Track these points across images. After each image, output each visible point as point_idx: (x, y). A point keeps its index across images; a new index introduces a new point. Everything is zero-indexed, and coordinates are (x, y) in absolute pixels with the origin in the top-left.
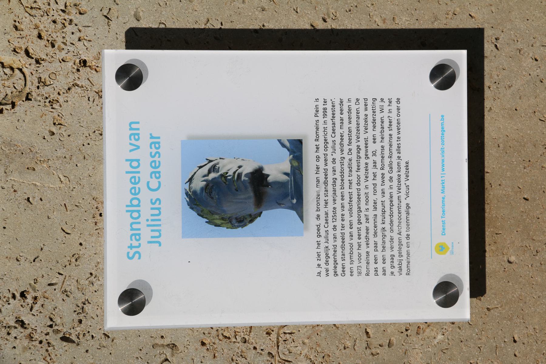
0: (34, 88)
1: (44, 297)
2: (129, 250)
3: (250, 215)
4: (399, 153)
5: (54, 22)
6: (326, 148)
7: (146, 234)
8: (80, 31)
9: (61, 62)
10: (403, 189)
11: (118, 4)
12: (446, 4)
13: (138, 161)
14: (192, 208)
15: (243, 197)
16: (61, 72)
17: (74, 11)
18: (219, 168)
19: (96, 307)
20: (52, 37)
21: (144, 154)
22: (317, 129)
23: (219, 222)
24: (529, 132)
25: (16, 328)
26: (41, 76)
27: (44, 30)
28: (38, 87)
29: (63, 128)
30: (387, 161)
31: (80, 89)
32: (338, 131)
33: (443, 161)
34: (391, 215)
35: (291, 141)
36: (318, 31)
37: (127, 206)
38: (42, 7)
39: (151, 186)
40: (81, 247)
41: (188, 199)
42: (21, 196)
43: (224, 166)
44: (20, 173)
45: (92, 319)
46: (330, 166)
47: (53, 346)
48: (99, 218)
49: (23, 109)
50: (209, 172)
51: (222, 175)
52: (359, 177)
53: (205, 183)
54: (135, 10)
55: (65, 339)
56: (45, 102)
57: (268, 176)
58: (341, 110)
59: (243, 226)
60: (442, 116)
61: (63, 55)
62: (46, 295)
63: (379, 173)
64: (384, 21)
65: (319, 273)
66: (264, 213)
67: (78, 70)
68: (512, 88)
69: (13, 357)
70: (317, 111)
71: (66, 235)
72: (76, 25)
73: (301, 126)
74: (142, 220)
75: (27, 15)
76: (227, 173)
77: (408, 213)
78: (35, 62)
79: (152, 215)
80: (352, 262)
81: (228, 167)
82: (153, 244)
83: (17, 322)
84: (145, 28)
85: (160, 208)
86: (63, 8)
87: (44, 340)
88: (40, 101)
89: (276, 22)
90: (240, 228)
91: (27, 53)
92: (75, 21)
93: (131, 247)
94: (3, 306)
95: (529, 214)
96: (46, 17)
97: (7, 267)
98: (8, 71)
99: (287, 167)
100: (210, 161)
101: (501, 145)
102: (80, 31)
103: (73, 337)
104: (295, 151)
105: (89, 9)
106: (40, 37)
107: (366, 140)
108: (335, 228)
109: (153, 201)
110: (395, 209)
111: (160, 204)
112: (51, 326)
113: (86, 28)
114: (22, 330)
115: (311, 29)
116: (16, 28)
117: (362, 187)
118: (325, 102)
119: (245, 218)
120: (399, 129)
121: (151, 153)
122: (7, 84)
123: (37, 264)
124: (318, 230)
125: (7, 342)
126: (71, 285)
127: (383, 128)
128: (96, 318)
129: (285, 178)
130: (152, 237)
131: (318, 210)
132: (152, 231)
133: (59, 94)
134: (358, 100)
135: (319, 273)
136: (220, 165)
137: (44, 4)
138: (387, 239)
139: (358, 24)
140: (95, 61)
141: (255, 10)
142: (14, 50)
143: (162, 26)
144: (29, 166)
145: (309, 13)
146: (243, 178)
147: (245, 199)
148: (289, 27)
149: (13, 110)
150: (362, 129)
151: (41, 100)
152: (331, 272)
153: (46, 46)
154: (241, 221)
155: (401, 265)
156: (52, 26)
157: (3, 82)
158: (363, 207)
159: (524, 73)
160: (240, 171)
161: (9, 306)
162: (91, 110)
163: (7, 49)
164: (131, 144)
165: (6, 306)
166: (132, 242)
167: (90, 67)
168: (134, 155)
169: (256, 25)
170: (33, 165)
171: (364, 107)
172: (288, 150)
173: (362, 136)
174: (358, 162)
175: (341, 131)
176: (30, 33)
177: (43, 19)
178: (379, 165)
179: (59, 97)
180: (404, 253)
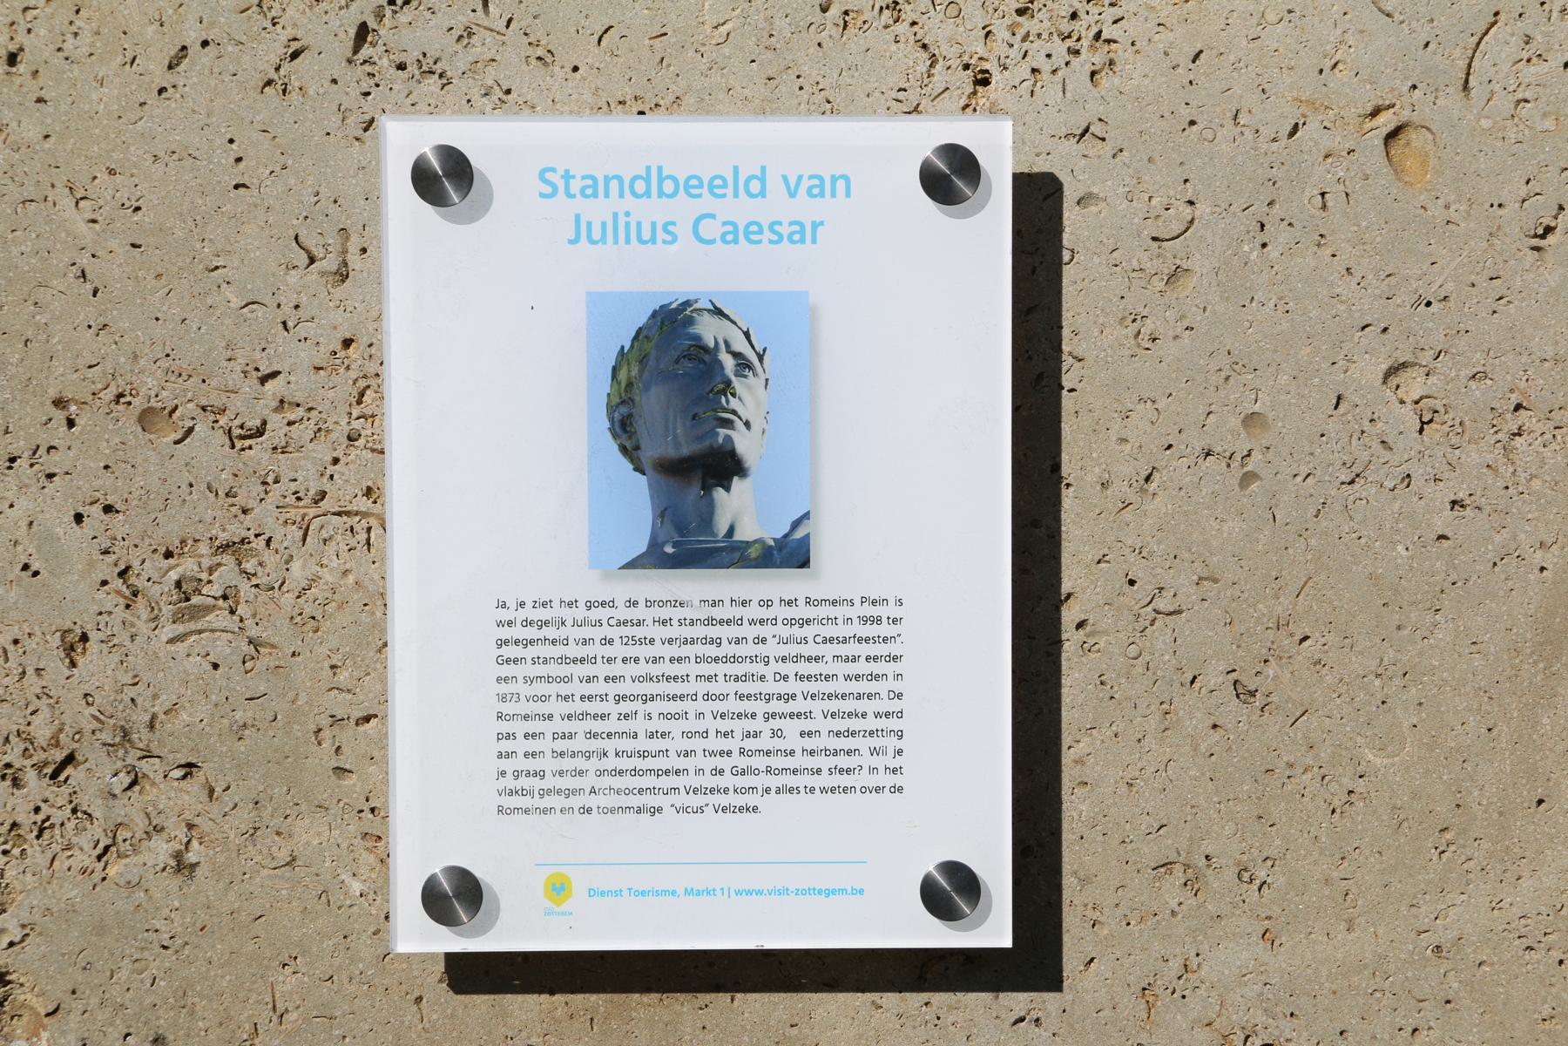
2: (561, 172)
3: (637, 448)
4: (778, 791)
5: (1074, 16)
6: (790, 622)
7: (597, 211)
10: (698, 800)
13: (763, 193)
14: (654, 314)
16: (962, 29)
17: (1099, 59)
19: (433, 102)
21: (777, 207)
22: (834, 603)
23: (623, 375)
29: (836, 32)
30: (760, 762)
32: (829, 650)
33: (759, 892)
34: (635, 772)
35: (805, 542)
36: (1058, 609)
37: (660, 169)
40: (568, 69)
41: (674, 306)
43: (749, 388)
51: (728, 383)
52: (723, 697)
53: (712, 344)
57: (728, 489)
58: (875, 659)
59: (612, 430)
60: (861, 891)
61: (1001, 33)
63: (733, 744)
65: (504, 605)
66: (642, 480)
67: (966, 67)
70: (874, 603)
71: (596, 37)
73: (838, 566)
74: (629, 202)
76: (734, 395)
79: (639, 224)
80: (529, 680)
81: (748, 398)
84: (1061, 218)
86: (1104, 36)
90: (608, 425)
92: (1075, 61)
93: (567, 176)
99: (745, 533)
100: (761, 358)
101: (795, 1031)
103: (366, 51)
107: (808, 715)
109: (671, 228)
110: (648, 781)
117: (701, 706)
119: (631, 435)
120: (833, 790)
121: (780, 223)
124: (603, 604)
126: (483, 46)
129: (722, 529)
130: (589, 224)
131: (649, 603)
132: (604, 225)
133: (914, 23)
134: (899, 696)
135: (504, 605)
136: (751, 379)
143: (1066, 258)
146: (722, 432)
148: (1064, 544)
150: (834, 705)
152: (506, 633)
154: (624, 426)
155: (521, 794)
160: (739, 424)
162: (877, 94)
164: (800, 178)
167: (975, 93)
172: (786, 536)
173: (817, 707)
174: (756, 697)
175: (829, 658)
178: (750, 744)
179: (906, 24)
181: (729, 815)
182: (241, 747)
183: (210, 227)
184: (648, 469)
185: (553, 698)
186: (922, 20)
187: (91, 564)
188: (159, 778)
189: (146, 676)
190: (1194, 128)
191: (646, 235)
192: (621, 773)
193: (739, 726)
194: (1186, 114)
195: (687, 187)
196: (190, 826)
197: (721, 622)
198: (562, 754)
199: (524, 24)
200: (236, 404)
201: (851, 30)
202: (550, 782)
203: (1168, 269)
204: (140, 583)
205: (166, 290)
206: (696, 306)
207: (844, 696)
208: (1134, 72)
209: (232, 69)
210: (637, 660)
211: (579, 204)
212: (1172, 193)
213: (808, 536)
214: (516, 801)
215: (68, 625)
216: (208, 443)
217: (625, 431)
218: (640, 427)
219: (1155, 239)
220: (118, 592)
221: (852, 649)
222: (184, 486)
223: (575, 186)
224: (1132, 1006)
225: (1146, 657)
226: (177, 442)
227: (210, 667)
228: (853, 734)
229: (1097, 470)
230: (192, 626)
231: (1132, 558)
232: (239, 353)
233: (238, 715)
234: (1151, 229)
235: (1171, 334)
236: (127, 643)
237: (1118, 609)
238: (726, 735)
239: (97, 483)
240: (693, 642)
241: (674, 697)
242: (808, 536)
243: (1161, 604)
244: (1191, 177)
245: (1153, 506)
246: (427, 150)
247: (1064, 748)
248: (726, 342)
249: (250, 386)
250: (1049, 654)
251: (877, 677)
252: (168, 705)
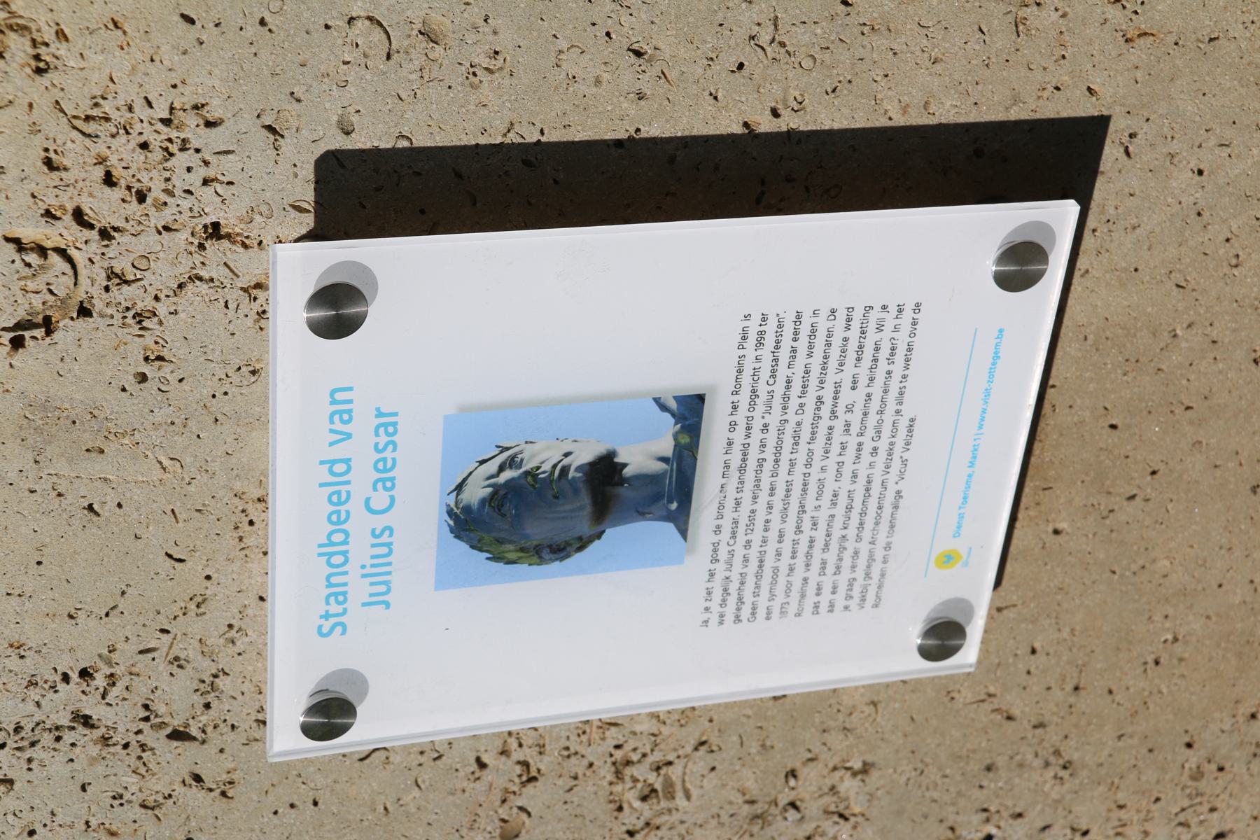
0: (96, 291)
1: (131, 674)
3: (580, 538)
4: (900, 403)
5: (144, 146)
7: (359, 589)
9: (160, 233)
10: (896, 465)
13: (347, 461)
14: (457, 537)
15: (567, 507)
16: (161, 255)
17: (192, 120)
18: (522, 460)
19: (240, 680)
20: (139, 181)
21: (361, 449)
22: (740, 372)
24: (1149, 310)
25: (73, 728)
26: (113, 263)
27: (119, 166)
28: (107, 289)
29: (167, 368)
30: (872, 420)
31: (205, 286)
32: (782, 371)
33: (984, 411)
34: (863, 513)
37: (320, 546)
38: (114, 115)
39: (373, 505)
40: (208, 583)
41: (452, 523)
42: (74, 502)
43: (533, 456)
44: (70, 461)
46: (756, 435)
47: (152, 749)
48: (248, 528)
49: (71, 335)
50: (501, 468)
51: (527, 473)
52: (811, 453)
53: (490, 490)
54: (340, 112)
55: (177, 735)
56: (125, 317)
57: (625, 465)
58: (796, 333)
59: (562, 559)
60: (1001, 331)
61: (167, 216)
62: (134, 670)
63: (852, 442)
64: (905, 110)
65: (706, 622)
67: (202, 247)
68: (1138, 231)
70: (744, 338)
71: (177, 565)
74: (353, 567)
76: (538, 468)
77: (896, 507)
78: (98, 237)
79: (373, 557)
80: (772, 597)
81: (542, 455)
84: (363, 151)
85: (391, 543)
86: (166, 115)
87: (134, 743)
88: (112, 317)
89: (667, 121)
91: (78, 215)
92: (195, 143)
93: (327, 616)
94: (44, 696)
96: (123, 138)
98: (33, 258)
99: (666, 446)
101: (1091, 337)
102: (206, 163)
103: (194, 731)
104: (687, 415)
105: (229, 115)
106: (109, 180)
107: (838, 385)
108: (748, 544)
109: (377, 532)
110: (873, 504)
111: (391, 535)
112: (146, 719)
113: (221, 157)
114: (86, 731)
115: (743, 135)
116: (48, 163)
118: (764, 320)
119: (568, 544)
120: (907, 360)
122: (31, 285)
123: (115, 619)
124: (715, 551)
125: (56, 753)
126: (189, 650)
127: (875, 360)
129: (662, 466)
130: (371, 595)
132: (372, 584)
133: (157, 298)
134: (833, 311)
135: (706, 622)
136: (525, 455)
137: (118, 109)
138: (847, 555)
139: (847, 119)
140: (242, 226)
141: (622, 99)
143: (406, 144)
145: (743, 99)
146: (572, 474)
147: (572, 511)
149: (48, 340)
151: (115, 313)
152: (729, 618)
153: (123, 200)
154: (559, 550)
155: (867, 593)
156: (140, 156)
157: (23, 283)
158: (810, 503)
159: (1170, 200)
160: (566, 461)
161: (56, 696)
163: (29, 213)
164: (332, 431)
165: (51, 695)
166: (328, 608)
168: (340, 451)
169: (621, 132)
170: (99, 443)
171: (844, 324)
172: (673, 415)
173: (831, 378)
174: (814, 426)
175: (789, 372)
176: (83, 175)
177: (115, 143)
178: (855, 429)
179: (157, 305)
180: (875, 573)
182: (778, 746)
183: (351, 817)
186: (152, 291)
188: (794, 793)
189: (715, 810)
190: (268, 19)
191: (385, 550)
192: (861, 524)
193: (838, 437)
194: (252, 30)
195: (339, 522)
197: (744, 460)
198: (838, 568)
199: (165, 621)
200: (501, 782)
201: (165, 353)
202: (860, 574)
203: (422, 43)
204: (640, 824)
206: (452, 504)
207: (826, 357)
208: (207, 82)
209: (211, 821)
210: (767, 521)
211: (353, 605)
212: (340, 42)
217: (564, 549)
218: (560, 538)
219: (389, 57)
221: (784, 354)
222: (566, 807)
223: (334, 608)
224: (1140, 52)
225: (815, 51)
226: (529, 814)
227: (713, 773)
228: (861, 347)
229: (625, 105)
230: (678, 787)
231: (716, 67)
232: (459, 786)
233: (753, 751)
234: (378, 62)
235: (491, 37)
236: (686, 825)
237: (765, 79)
238: (843, 448)
240: (758, 480)
241: (804, 490)
243: (764, 39)
244: (322, 22)
245: (667, 52)
246: (302, 719)
247: (890, 124)
248: (488, 478)
249: (487, 775)
250: (799, 142)
251: (813, 332)
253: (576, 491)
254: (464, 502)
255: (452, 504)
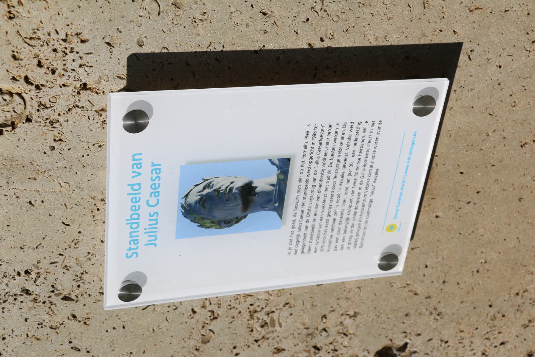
0: (34, 111)
2: (128, 252)
3: (237, 218)
4: (373, 163)
5: (55, 50)
6: (310, 163)
7: (143, 238)
8: (81, 58)
9: (61, 87)
10: (370, 188)
11: (121, 32)
12: (436, 22)
13: (139, 185)
14: (185, 217)
15: (232, 205)
16: (62, 96)
17: (75, 40)
18: (213, 185)
19: (93, 276)
20: (52, 65)
21: (145, 179)
22: (305, 149)
24: (478, 124)
25: (22, 295)
28: (38, 110)
30: (361, 169)
31: (80, 110)
33: (408, 166)
34: (356, 208)
35: (280, 160)
36: (315, 49)
37: (127, 220)
38: (42, 37)
39: (151, 203)
40: (80, 235)
41: (183, 211)
42: (23, 200)
43: (218, 183)
44: (22, 183)
45: (89, 284)
47: (55, 304)
48: (97, 212)
49: (23, 130)
50: (204, 188)
51: (215, 190)
52: (334, 183)
53: (199, 197)
54: (138, 37)
56: (46, 123)
57: (256, 187)
58: (329, 133)
59: (229, 226)
60: (415, 133)
61: (64, 80)
62: (48, 271)
63: (352, 178)
64: (376, 39)
66: (249, 215)
67: (79, 93)
68: (473, 91)
69: (20, 315)
70: (307, 135)
71: (66, 227)
72: (77, 53)
73: (289, 146)
74: (141, 229)
75: (26, 45)
76: (220, 188)
80: (317, 243)
81: (222, 183)
82: (149, 246)
83: (22, 291)
85: (157, 219)
86: (64, 37)
87: (47, 301)
88: (40, 122)
89: (276, 43)
90: (227, 228)
91: (26, 79)
92: (76, 49)
93: (130, 249)
95: (460, 184)
96: (46, 47)
97: (11, 254)
98: (7, 97)
99: (274, 180)
101: (453, 136)
102: (81, 58)
103: (73, 297)
105: (91, 38)
106: (40, 65)
107: (346, 155)
108: (308, 221)
109: (152, 214)
110: (360, 205)
112: (53, 291)
113: (88, 56)
114: (27, 296)
115: (308, 49)
116: (14, 57)
117: (336, 190)
118: (316, 127)
119: (232, 220)
120: (376, 145)
121: (152, 178)
122: (6, 109)
124: (294, 224)
126: (71, 262)
128: (92, 283)
129: (272, 188)
130: (149, 241)
131: (296, 209)
132: (149, 236)
133: (59, 115)
134: (345, 124)
136: (214, 183)
137: (44, 35)
138: (349, 226)
139: (352, 42)
141: (257, 33)
142: (14, 78)
143: (166, 51)
144: (30, 177)
145: (309, 34)
146: (234, 191)
147: (234, 206)
148: (288, 47)
150: (344, 146)
151: (41, 121)
152: (299, 252)
154: (228, 223)
155: (357, 242)
156: (53, 54)
157: (2, 107)
159: (487, 78)
160: (232, 185)
161: (15, 281)
162: (91, 127)
163: (6, 78)
164: (133, 172)
165: (12, 281)
167: (90, 89)
170: (34, 175)
171: (349, 129)
172: (277, 167)
173: (344, 151)
175: (326, 149)
176: (29, 62)
177: (42, 49)
178: (353, 173)
180: (361, 234)
181: (378, 178)
183: (139, 333)
184: (245, 214)
185: (325, 235)
187: (252, 350)
189: (292, 332)
191: (155, 222)
192: (355, 213)
193: (346, 176)
195: (135, 210)
196: (342, 315)
197: (306, 186)
198: (345, 231)
200: (202, 319)
201: (63, 138)
202: (354, 234)
203: (173, 8)
204: (260, 337)
205: (161, 343)
206: (183, 203)
207: (341, 143)
208: (82, 24)
209: (80, 334)
212: (138, 7)
213: (278, 159)
214: (359, 244)
215: (271, 353)
216: (215, 325)
217: (230, 222)
218: (229, 218)
219: (159, 14)
220: (263, 342)
221: (324, 142)
223: (133, 246)
225: (339, 14)
227: (291, 316)
228: (356, 139)
229: (259, 36)
230: (277, 322)
231: (297, 20)
233: (308, 307)
234: (155, 16)
235: (202, 6)
237: (318, 25)
238: (348, 181)
239: (226, 352)
241: (332, 199)
242: (278, 159)
246: (119, 292)
247: (370, 45)
248: (199, 192)
249: (196, 316)
251: (336, 133)
252: (302, 326)
253: (236, 198)
254: (189, 202)
255: (183, 203)
